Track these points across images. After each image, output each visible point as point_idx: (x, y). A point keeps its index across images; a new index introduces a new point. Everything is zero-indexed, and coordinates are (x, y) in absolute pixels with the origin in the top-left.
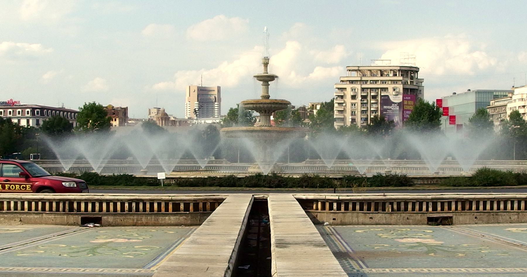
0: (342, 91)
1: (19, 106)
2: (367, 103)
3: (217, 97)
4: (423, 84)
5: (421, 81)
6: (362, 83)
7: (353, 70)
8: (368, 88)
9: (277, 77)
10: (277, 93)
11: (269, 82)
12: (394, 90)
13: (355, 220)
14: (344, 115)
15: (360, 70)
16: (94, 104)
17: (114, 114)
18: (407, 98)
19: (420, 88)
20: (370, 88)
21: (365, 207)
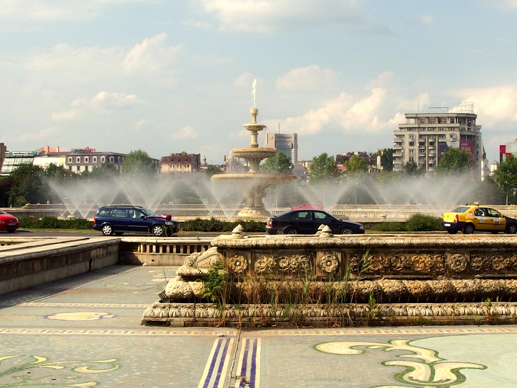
0: (400, 138)
1: (95, 153)
2: (425, 149)
3: (293, 143)
4: (481, 131)
5: (479, 127)
6: (420, 130)
7: (411, 118)
8: (425, 135)
9: (265, 127)
11: (258, 132)
12: (451, 136)
13: (171, 261)
14: (402, 162)
15: (418, 118)
16: (140, 152)
17: (187, 160)
18: (464, 144)
19: (478, 135)
20: (428, 135)
21: (182, 250)
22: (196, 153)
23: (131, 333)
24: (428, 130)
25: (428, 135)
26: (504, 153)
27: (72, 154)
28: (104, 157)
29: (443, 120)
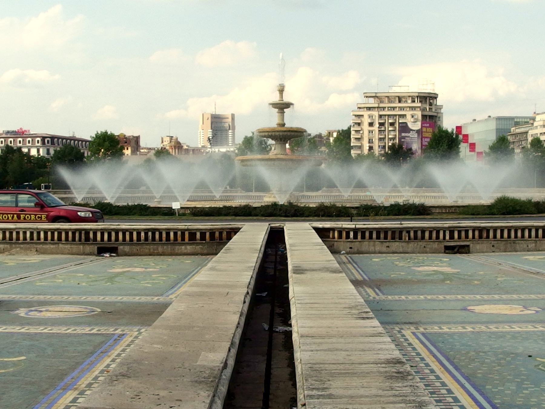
0: (359, 118)
1: (29, 134)
2: (385, 130)
3: (231, 124)
4: (442, 111)
5: (441, 107)
6: (379, 109)
8: (385, 115)
9: (292, 104)
10: (292, 121)
11: (285, 110)
12: (413, 117)
15: (377, 97)
17: (126, 142)
18: (425, 125)
19: (439, 115)
22: (136, 135)
23: (98, 331)
24: (388, 110)
25: (388, 115)
26: (461, 134)
27: (4, 136)
28: (39, 139)
29: (404, 100)
